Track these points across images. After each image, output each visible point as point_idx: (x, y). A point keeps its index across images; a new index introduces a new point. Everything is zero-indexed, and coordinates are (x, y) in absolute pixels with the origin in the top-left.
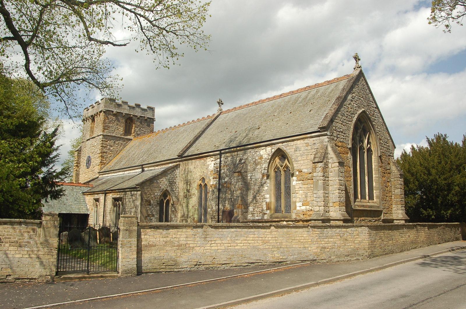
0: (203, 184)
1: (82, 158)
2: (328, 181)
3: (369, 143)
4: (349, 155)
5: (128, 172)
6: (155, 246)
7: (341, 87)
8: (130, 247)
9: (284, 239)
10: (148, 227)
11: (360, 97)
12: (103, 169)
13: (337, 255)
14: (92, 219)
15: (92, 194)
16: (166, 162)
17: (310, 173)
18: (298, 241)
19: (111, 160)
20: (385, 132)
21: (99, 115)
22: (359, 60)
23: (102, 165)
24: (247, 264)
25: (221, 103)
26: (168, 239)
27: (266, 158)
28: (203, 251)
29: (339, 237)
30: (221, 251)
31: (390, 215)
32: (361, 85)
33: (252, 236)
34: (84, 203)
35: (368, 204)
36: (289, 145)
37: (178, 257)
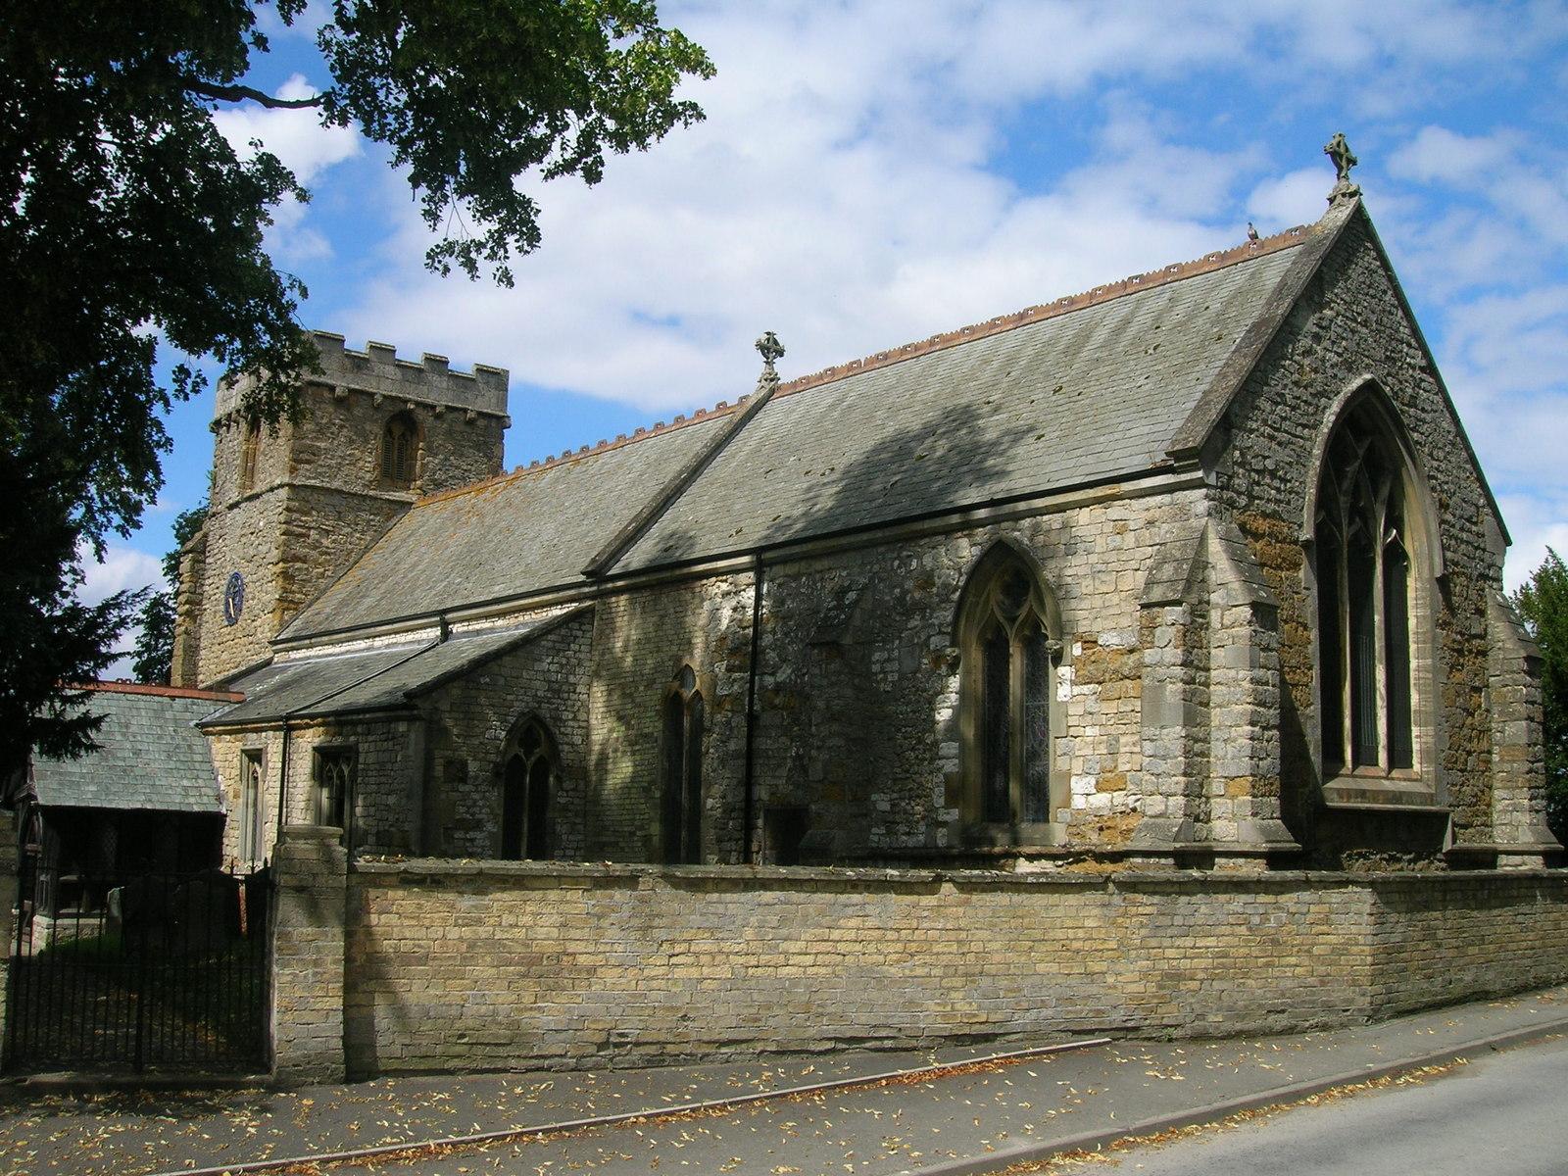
1: (207, 582)
4: (1301, 574)
5: (386, 640)
6: (424, 960)
7: (1272, 278)
10: (394, 880)
11: (1355, 320)
12: (292, 628)
13: (1230, 1009)
16: (537, 599)
17: (1131, 651)
18: (1058, 946)
19: (324, 591)
20: (1463, 475)
22: (1352, 162)
23: (288, 609)
24: (830, 1045)
25: (776, 351)
26: (483, 932)
29: (1243, 930)
30: (714, 985)
31: (1482, 833)
32: (1360, 270)
34: (205, 766)
35: (1387, 785)
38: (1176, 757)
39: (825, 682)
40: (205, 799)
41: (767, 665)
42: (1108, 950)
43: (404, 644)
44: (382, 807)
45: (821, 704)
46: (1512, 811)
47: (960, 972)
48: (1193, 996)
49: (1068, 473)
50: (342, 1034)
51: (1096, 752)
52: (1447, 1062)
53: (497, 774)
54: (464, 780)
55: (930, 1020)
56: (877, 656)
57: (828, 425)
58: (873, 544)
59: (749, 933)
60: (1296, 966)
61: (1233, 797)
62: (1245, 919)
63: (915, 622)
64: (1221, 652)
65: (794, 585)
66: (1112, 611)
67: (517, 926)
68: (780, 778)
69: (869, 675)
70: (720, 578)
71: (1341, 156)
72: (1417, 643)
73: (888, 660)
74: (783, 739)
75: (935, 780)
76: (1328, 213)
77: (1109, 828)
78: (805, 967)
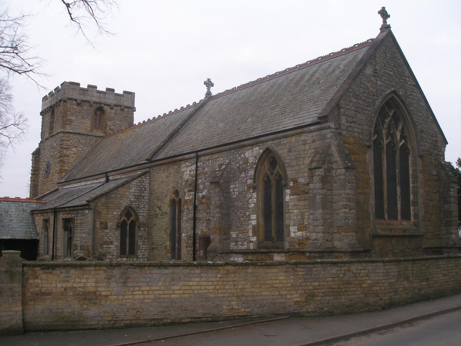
0: (177, 199)
3: (402, 137)
6: (50, 294)
8: (13, 296)
21: (59, 105)
24: (189, 320)
26: (69, 285)
30: (148, 301)
33: (198, 279)
39: (215, 195)
40: (33, 235)
41: (200, 190)
42: (287, 287)
44: (82, 238)
45: (213, 203)
47: (235, 295)
50: (22, 318)
51: (298, 218)
52: (410, 322)
53: (118, 226)
54: (106, 228)
56: (232, 186)
58: (230, 149)
61: (340, 233)
62: (337, 276)
63: (243, 175)
64: (335, 185)
65: (207, 163)
66: (302, 171)
68: (204, 226)
69: (229, 193)
70: (186, 161)
72: (412, 178)
73: (235, 188)
74: (204, 214)
75: (249, 227)
77: (302, 243)
78: (180, 294)
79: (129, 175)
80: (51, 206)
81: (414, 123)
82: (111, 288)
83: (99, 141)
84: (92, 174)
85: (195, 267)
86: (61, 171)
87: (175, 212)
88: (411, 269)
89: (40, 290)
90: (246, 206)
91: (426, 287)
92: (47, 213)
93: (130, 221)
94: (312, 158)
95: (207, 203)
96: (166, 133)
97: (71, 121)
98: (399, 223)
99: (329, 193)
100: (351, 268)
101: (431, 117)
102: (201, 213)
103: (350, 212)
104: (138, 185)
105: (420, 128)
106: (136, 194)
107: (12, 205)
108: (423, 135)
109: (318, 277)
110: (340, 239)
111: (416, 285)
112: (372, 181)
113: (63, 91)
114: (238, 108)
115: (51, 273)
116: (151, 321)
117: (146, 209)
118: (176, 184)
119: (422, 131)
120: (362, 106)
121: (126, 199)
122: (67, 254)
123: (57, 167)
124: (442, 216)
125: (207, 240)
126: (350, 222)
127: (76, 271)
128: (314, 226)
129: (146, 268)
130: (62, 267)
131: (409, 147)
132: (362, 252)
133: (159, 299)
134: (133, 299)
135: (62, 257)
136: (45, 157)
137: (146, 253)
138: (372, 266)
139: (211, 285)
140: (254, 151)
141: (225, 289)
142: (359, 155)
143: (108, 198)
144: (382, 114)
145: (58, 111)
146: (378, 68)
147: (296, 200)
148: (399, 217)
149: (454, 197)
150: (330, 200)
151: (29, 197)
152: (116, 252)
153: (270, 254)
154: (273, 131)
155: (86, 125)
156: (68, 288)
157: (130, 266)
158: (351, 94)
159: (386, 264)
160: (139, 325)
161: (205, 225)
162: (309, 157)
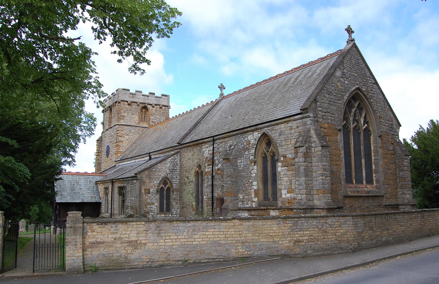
0: (199, 171)
2: (311, 167)
3: (365, 122)
5: (138, 160)
6: (103, 243)
8: (76, 245)
9: (250, 233)
13: (314, 249)
14: (104, 207)
15: (103, 183)
21: (115, 105)
24: (207, 261)
25: (223, 88)
26: (118, 236)
27: (253, 144)
28: (156, 247)
30: (176, 246)
33: (212, 230)
36: (274, 129)
37: (129, 254)
38: (303, 185)
39: (226, 168)
40: (97, 199)
42: (279, 235)
43: (142, 161)
44: (131, 200)
45: (226, 173)
46: (402, 195)
47: (240, 242)
48: (303, 246)
49: (280, 115)
50: (82, 262)
54: (149, 193)
55: (233, 254)
56: (239, 161)
57: (233, 105)
58: (237, 134)
59: (185, 234)
60: (332, 238)
61: (318, 195)
62: (317, 227)
63: (247, 153)
64: (314, 158)
65: (221, 145)
67: (126, 234)
68: (219, 191)
69: (237, 166)
71: (349, 31)
73: (241, 162)
75: (252, 191)
76: (346, 46)
77: (290, 202)
78: (200, 241)
79: (165, 154)
80: (110, 178)
81: (374, 111)
82: (149, 237)
83: (145, 130)
84: (140, 154)
85: (210, 221)
86: (117, 153)
87: (199, 181)
88: (374, 221)
89: (96, 240)
90: (249, 176)
91: (386, 235)
92: (107, 183)
93: (166, 187)
94: (297, 139)
95: (221, 174)
96: (191, 123)
97: (124, 117)
98: (365, 186)
99: (310, 165)
100: (327, 221)
101: (388, 107)
102: (217, 181)
103: (326, 179)
104: (172, 162)
105: (379, 115)
106: (171, 168)
107: (82, 178)
108: (382, 120)
109: (302, 227)
110: (319, 199)
111: (378, 233)
112: (343, 155)
113: (117, 95)
114: (243, 104)
115: (104, 227)
116: (178, 262)
117: (178, 179)
118: (199, 160)
119: (380, 118)
120: (333, 100)
121: (163, 172)
122: (122, 212)
123: (114, 150)
124: (398, 181)
125: (222, 201)
126: (326, 186)
127: (123, 225)
128: (299, 190)
129: (175, 222)
130: (113, 223)
131: (371, 129)
132: (336, 208)
133: (184, 245)
134: (165, 246)
135: (118, 215)
136: (106, 142)
137: (178, 211)
138: (343, 219)
139: (222, 235)
140: (254, 135)
141: (233, 237)
142: (332, 136)
143: (150, 171)
144: (349, 105)
145: (114, 110)
146: (346, 71)
147: (286, 170)
148: (364, 182)
149: (407, 167)
150: (311, 170)
151: (94, 171)
152: (156, 210)
153: (267, 210)
154: (268, 121)
155: (135, 119)
156: (117, 238)
157: (163, 221)
158: (325, 92)
159: (355, 218)
160: (169, 265)
161: (220, 189)
162: (295, 138)
